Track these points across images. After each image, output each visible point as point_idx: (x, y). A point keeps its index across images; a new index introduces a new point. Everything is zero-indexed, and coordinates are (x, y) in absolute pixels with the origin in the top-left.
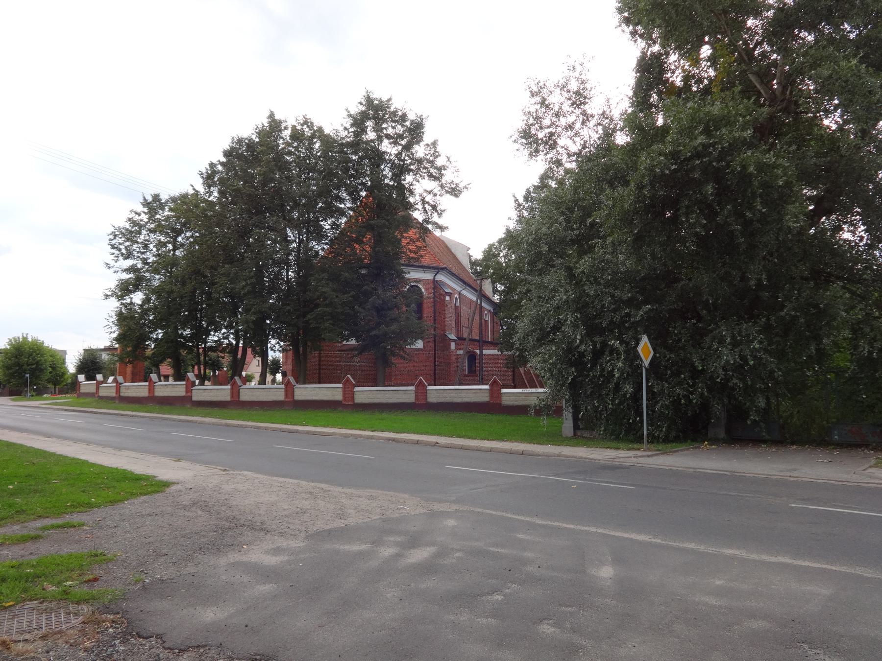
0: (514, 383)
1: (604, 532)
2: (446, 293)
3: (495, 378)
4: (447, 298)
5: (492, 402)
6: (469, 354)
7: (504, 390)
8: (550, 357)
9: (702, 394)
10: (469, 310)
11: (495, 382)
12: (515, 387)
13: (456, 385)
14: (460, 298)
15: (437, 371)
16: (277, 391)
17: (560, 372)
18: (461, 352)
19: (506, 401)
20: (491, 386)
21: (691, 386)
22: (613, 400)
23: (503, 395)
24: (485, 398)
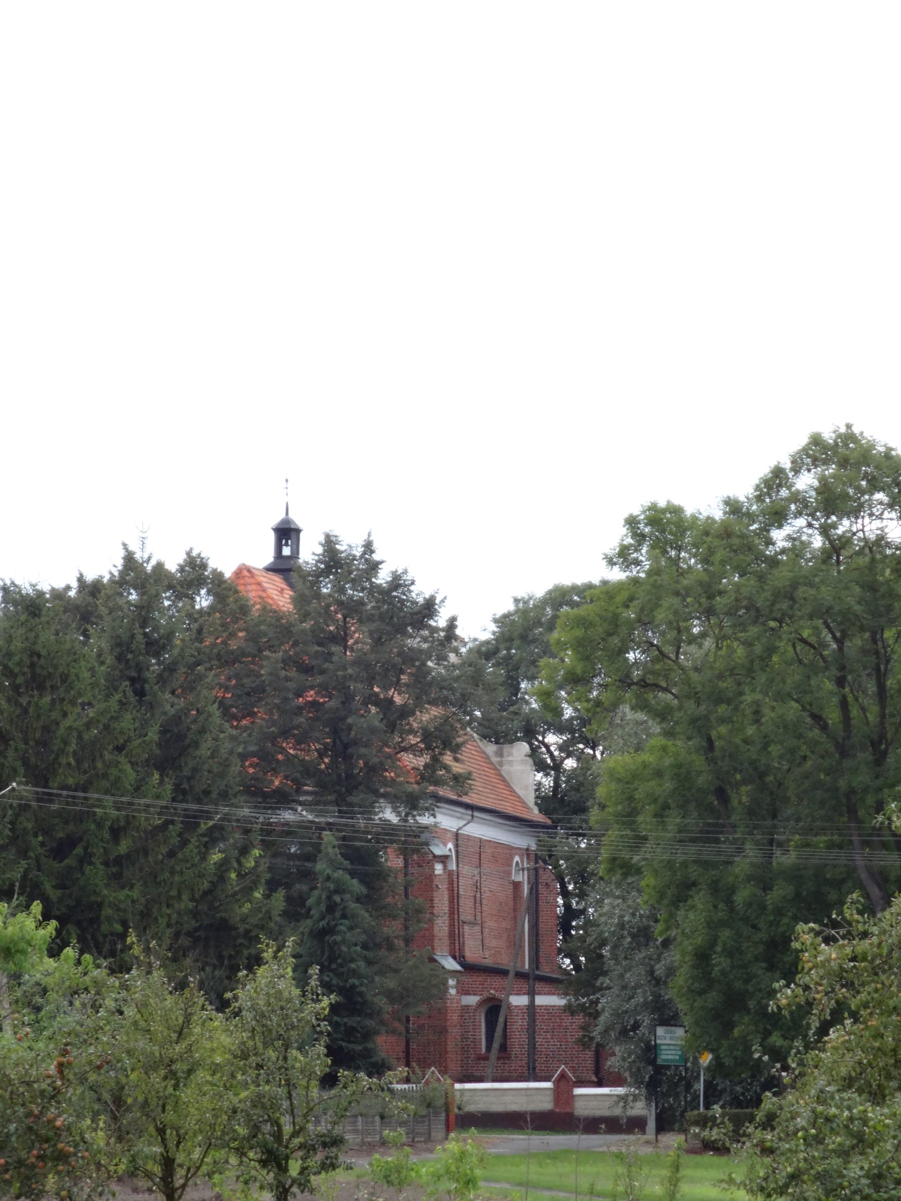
0: (597, 1076)
1: (367, 868)
2: (435, 856)
3: (563, 1070)
4: (439, 868)
5: (558, 1110)
6: (490, 1005)
7: (578, 1091)
8: (629, 1056)
9: (756, 1091)
10: (476, 872)
11: (563, 1076)
12: (600, 1084)
13: (487, 1081)
14: (457, 852)
15: (414, 1046)
16: (487, 1096)
17: (639, 1069)
18: (472, 1000)
19: (581, 1109)
20: (557, 1083)
21: (749, 1084)
22: (685, 1097)
23: (576, 1099)
24: (546, 1104)
